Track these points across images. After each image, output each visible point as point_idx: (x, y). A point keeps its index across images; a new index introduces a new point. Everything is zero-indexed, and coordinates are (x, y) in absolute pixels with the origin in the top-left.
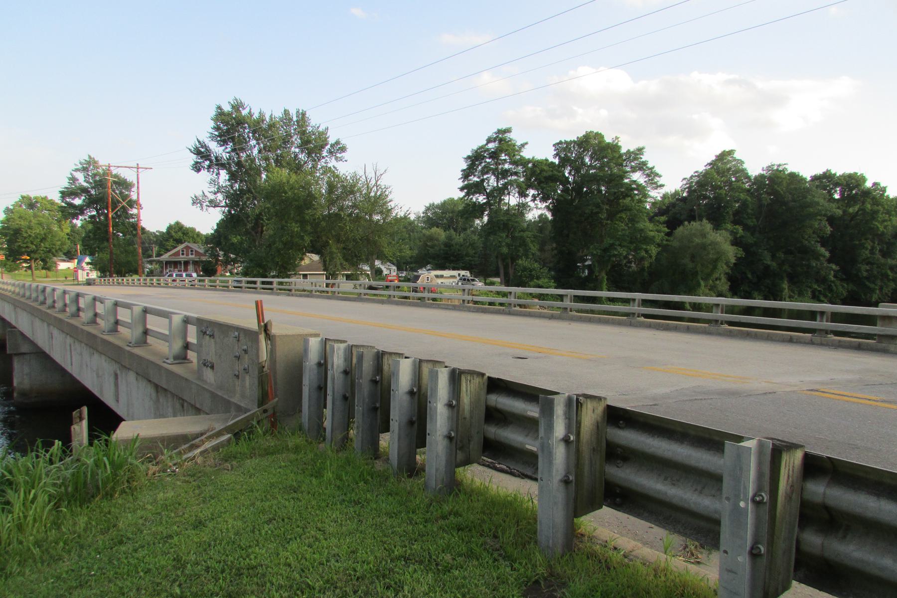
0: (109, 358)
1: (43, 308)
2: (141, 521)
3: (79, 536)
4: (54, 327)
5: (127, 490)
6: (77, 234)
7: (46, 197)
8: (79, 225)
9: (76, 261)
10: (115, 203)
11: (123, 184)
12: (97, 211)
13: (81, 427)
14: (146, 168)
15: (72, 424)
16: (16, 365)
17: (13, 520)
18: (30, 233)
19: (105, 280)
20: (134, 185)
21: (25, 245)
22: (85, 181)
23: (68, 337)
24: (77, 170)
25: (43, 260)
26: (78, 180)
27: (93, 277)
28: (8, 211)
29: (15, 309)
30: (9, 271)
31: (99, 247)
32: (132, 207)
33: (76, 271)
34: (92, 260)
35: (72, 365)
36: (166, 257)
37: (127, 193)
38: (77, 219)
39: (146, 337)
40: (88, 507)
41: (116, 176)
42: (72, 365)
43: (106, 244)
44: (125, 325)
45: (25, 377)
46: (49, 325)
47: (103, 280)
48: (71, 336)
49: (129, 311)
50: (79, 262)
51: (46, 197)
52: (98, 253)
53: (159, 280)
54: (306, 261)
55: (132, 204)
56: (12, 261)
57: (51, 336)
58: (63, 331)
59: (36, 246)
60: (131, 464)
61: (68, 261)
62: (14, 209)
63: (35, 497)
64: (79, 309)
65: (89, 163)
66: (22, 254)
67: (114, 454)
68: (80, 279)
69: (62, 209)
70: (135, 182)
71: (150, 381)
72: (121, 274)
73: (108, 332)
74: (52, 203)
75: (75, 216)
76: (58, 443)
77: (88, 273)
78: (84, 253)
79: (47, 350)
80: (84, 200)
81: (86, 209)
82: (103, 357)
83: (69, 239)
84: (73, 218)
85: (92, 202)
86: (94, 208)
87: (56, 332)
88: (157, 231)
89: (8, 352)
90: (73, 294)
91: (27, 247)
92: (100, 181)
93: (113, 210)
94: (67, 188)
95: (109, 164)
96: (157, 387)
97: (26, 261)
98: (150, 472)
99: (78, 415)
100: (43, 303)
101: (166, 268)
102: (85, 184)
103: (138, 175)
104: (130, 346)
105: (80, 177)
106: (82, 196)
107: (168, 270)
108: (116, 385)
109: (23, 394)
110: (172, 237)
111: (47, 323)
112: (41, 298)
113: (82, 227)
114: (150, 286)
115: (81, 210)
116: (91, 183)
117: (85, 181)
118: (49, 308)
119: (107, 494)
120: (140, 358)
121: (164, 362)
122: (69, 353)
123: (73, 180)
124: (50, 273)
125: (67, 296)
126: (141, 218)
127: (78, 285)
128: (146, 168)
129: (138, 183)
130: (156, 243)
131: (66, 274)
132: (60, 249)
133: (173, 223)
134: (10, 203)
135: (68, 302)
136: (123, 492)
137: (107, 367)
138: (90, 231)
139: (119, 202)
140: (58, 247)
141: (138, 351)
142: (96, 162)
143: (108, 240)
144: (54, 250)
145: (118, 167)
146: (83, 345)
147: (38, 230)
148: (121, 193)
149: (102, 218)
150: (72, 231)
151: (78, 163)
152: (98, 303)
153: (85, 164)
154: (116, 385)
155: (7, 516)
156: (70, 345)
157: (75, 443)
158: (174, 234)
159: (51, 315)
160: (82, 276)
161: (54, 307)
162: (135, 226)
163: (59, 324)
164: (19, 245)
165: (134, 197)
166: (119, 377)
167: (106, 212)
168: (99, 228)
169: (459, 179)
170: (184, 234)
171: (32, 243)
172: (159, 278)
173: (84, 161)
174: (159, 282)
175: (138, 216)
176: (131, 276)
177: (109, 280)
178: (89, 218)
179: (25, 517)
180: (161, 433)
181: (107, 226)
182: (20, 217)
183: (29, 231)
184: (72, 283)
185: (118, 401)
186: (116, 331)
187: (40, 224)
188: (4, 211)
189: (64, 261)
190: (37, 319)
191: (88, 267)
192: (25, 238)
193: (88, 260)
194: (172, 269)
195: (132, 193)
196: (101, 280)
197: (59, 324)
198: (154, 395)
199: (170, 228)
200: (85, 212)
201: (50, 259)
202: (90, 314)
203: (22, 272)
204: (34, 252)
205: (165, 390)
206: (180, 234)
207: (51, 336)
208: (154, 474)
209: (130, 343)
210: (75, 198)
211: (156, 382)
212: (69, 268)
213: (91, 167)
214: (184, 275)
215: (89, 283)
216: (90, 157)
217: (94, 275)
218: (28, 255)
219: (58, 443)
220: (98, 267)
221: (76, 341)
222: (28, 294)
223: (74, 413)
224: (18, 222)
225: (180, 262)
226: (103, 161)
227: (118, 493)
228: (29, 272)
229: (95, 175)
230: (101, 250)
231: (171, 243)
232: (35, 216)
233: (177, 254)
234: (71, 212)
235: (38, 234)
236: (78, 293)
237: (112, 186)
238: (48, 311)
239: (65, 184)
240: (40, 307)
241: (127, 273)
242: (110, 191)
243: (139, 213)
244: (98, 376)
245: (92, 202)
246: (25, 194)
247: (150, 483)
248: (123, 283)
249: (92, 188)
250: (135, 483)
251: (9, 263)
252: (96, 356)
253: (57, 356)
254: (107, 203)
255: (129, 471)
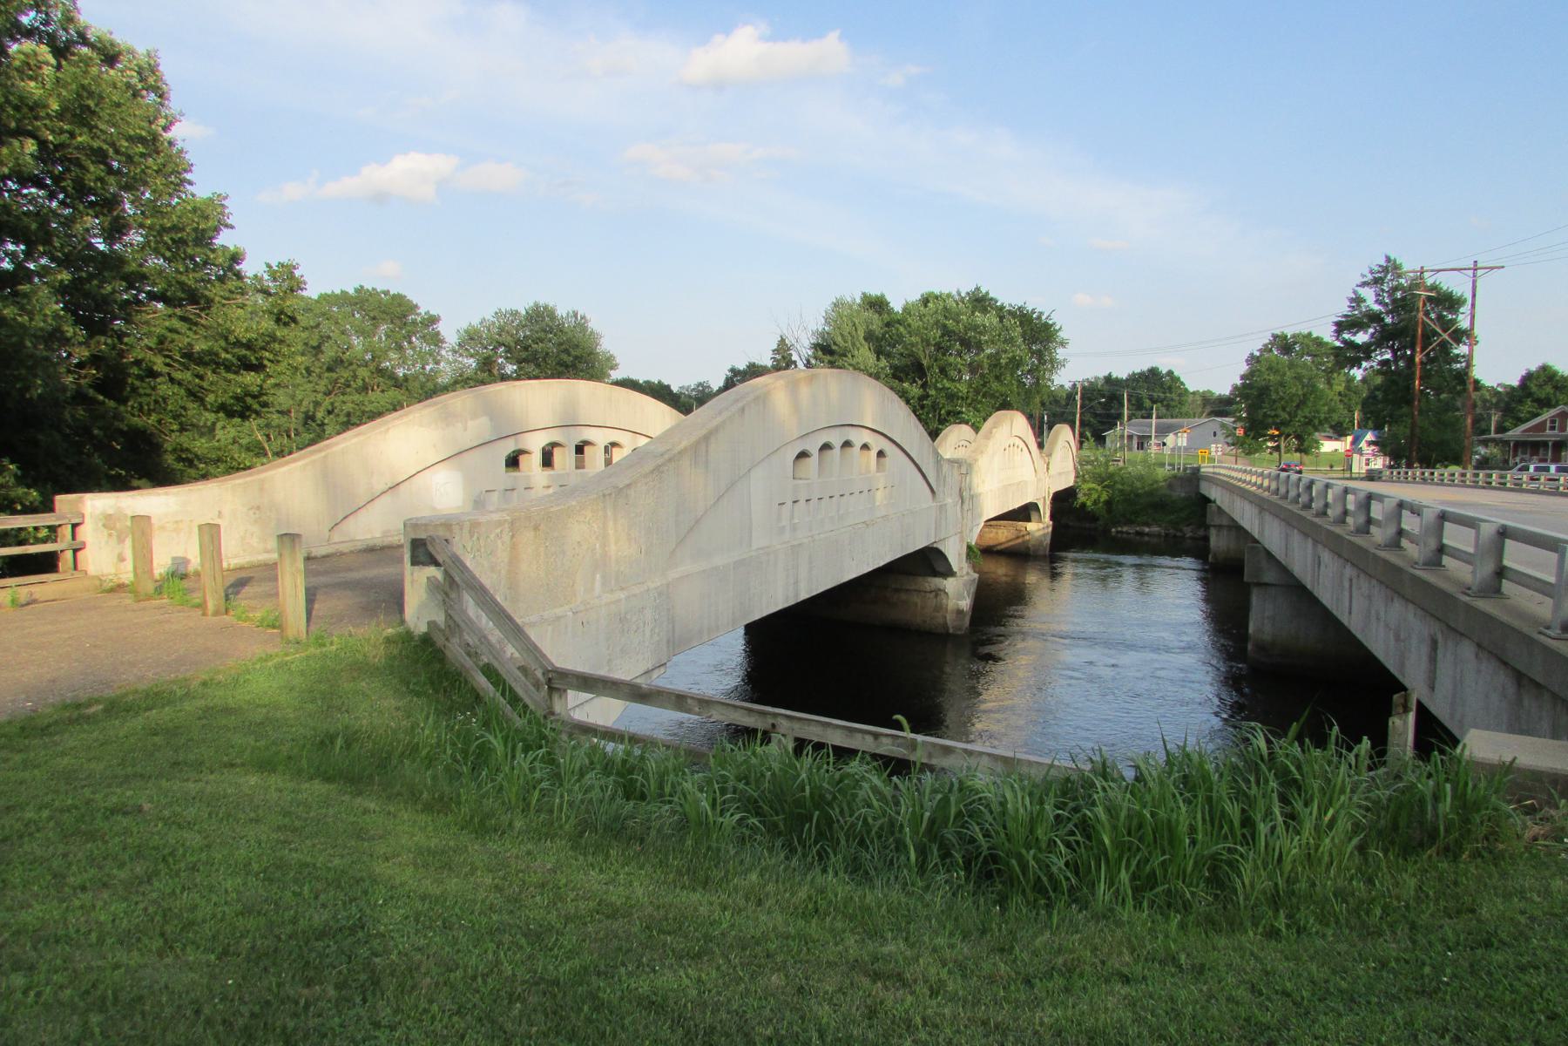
0: (1423, 609)
1: (1307, 515)
2: (1523, 919)
3: (1407, 907)
4: (1325, 546)
5: (1485, 854)
6: (1355, 393)
7: (1310, 334)
8: (1359, 378)
9: (1349, 438)
10: (1428, 336)
11: (1449, 302)
12: (1394, 352)
13: (1405, 723)
14: (1492, 268)
15: (1390, 715)
16: (1255, 599)
17: (1300, 845)
18: (1281, 394)
19: (1399, 473)
20: (1465, 301)
21: (1273, 413)
22: (1376, 301)
23: (1348, 567)
24: (1364, 284)
25: (1298, 437)
26: (1365, 301)
27: (1377, 467)
28: (1252, 359)
29: (1260, 512)
30: (1247, 454)
31: (1391, 416)
32: (1458, 341)
33: (1348, 456)
34: (1376, 437)
35: (1350, 613)
36: (1516, 433)
37: (1450, 317)
38: (1359, 368)
39: (1501, 582)
40: (1416, 862)
41: (1434, 288)
42: (1350, 613)
43: (1405, 410)
44: (1457, 554)
45: (1266, 621)
46: (1316, 542)
47: (1395, 473)
48: (1353, 564)
49: (1471, 532)
50: (1355, 442)
51: (1310, 334)
52: (1390, 426)
53: (1502, 477)
54: (1270, 432)
55: (1459, 336)
56: (1253, 438)
57: (1318, 562)
58: (1340, 556)
59: (1289, 414)
60: (1496, 809)
61: (1336, 439)
62: (1261, 355)
63: (1333, 820)
64: (1369, 521)
65: (1385, 270)
66: (1268, 427)
67: (1466, 784)
68: (1355, 469)
69: (1337, 352)
70: (1468, 296)
71: (1505, 664)
72: (1428, 463)
73: (1425, 564)
74: (1319, 342)
75: (1356, 362)
76: (1366, 743)
77: (1368, 460)
78: (1363, 425)
79: (1308, 582)
80: (1372, 335)
81: (1375, 350)
82: (1411, 606)
83: (1341, 401)
84: (1352, 367)
85: (1386, 336)
86: (1388, 347)
87: (1326, 556)
88: (1498, 385)
89: (1245, 579)
90: (1362, 495)
91: (1276, 416)
92: (1403, 299)
93: (1422, 350)
94: (1346, 316)
95: (1422, 268)
96: (1520, 678)
97: (1272, 438)
98: (1528, 835)
99: (1402, 701)
100: (1308, 506)
101: (1515, 455)
102: (1376, 307)
103: (1474, 282)
104: (1469, 595)
105: (1369, 294)
106: (1369, 327)
107: (1518, 460)
108: (1433, 660)
109: (1262, 647)
110: (1530, 395)
111: (1313, 539)
112: (1304, 499)
113: (1364, 380)
114: (1484, 488)
115: (1366, 351)
116: (1386, 304)
117: (1376, 301)
118: (1318, 515)
119: (1447, 849)
120: (1489, 618)
121: (1540, 633)
122: (1346, 594)
123: (1357, 300)
124: (1306, 458)
125: (1350, 497)
126: (1474, 362)
127: (1351, 479)
128: (1492, 268)
129: (1474, 296)
130: (1496, 406)
131: (1332, 457)
132: (1326, 419)
133: (1533, 368)
134: (1255, 346)
135: (1351, 507)
136: (1476, 854)
137: (1418, 627)
138: (1377, 388)
139: (1435, 334)
140: (1323, 416)
141: (1482, 605)
142: (1396, 267)
143: (1409, 403)
144: (1316, 422)
145: (1439, 271)
146: (1374, 582)
147: (1296, 390)
148: (1440, 317)
149: (1401, 364)
150: (1348, 388)
151: (1366, 272)
152: (1405, 513)
153: (1379, 272)
154: (1433, 660)
155: (1292, 840)
156: (1351, 580)
157: (1393, 749)
158: (1534, 389)
159: (1320, 526)
160: (1359, 466)
161: (1325, 514)
162: (1462, 377)
163: (1336, 545)
164: (1265, 413)
165: (1463, 323)
166: (1439, 645)
167: (1409, 353)
168: (1394, 382)
169: (232, 227)
170: (1556, 388)
171: (1284, 409)
172: (1503, 472)
173: (1376, 269)
174: (1502, 481)
175: (1469, 359)
176: (1446, 467)
177: (1407, 473)
178: (1378, 364)
179: (1317, 847)
180: (1551, 765)
181: (1411, 377)
182: (1270, 369)
183: (1280, 389)
184: (1341, 476)
185: (1432, 688)
186: (1439, 564)
187: (1298, 378)
188: (1247, 360)
189: (1330, 438)
190: (1296, 531)
191: (1368, 450)
192: (1274, 401)
193: (1369, 436)
194: (1527, 456)
195: (1460, 317)
196: (1392, 473)
197: (1336, 545)
198: (1511, 690)
199: (1527, 378)
200: (1373, 355)
201: (1309, 434)
202: (1391, 531)
203: (1266, 455)
204: (1284, 423)
205: (1538, 685)
206: (1549, 389)
207: (1318, 562)
208: (1535, 839)
209: (1469, 589)
210: (1357, 332)
211: (1518, 666)
212: (1336, 450)
213: (1389, 277)
214: (1553, 468)
215: (1372, 476)
216: (1388, 259)
217: (1379, 463)
218: (1277, 429)
219: (1366, 743)
220: (1388, 449)
221: (1362, 575)
222: (1283, 490)
223: (1395, 697)
224: (1266, 376)
225: (1545, 444)
226: (1409, 265)
227: (1467, 853)
228: (1276, 455)
229: (1395, 289)
230: (1393, 420)
231: (1528, 406)
232: (1291, 365)
233: (1540, 427)
234: (1349, 355)
235: (1294, 395)
236: (1370, 493)
237: (1424, 305)
238: (1317, 520)
239: (1343, 308)
240: (1303, 513)
241: (1439, 462)
242: (1421, 315)
243: (1471, 351)
244: (1397, 638)
245: (1386, 336)
246: (1278, 332)
247: (1530, 853)
248: (1464, 481)
249: (1387, 313)
250: (1501, 846)
251: (1249, 441)
252: (1398, 606)
253: (1326, 598)
254: (1414, 337)
255: (1489, 820)
